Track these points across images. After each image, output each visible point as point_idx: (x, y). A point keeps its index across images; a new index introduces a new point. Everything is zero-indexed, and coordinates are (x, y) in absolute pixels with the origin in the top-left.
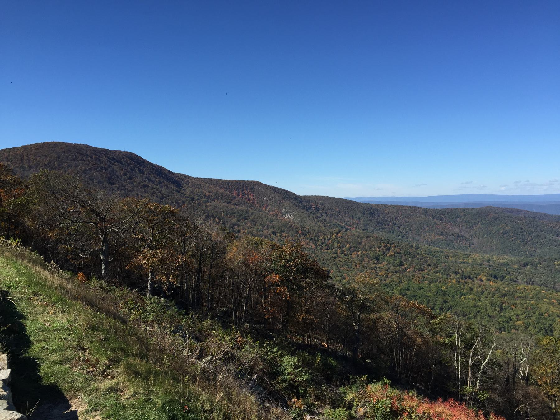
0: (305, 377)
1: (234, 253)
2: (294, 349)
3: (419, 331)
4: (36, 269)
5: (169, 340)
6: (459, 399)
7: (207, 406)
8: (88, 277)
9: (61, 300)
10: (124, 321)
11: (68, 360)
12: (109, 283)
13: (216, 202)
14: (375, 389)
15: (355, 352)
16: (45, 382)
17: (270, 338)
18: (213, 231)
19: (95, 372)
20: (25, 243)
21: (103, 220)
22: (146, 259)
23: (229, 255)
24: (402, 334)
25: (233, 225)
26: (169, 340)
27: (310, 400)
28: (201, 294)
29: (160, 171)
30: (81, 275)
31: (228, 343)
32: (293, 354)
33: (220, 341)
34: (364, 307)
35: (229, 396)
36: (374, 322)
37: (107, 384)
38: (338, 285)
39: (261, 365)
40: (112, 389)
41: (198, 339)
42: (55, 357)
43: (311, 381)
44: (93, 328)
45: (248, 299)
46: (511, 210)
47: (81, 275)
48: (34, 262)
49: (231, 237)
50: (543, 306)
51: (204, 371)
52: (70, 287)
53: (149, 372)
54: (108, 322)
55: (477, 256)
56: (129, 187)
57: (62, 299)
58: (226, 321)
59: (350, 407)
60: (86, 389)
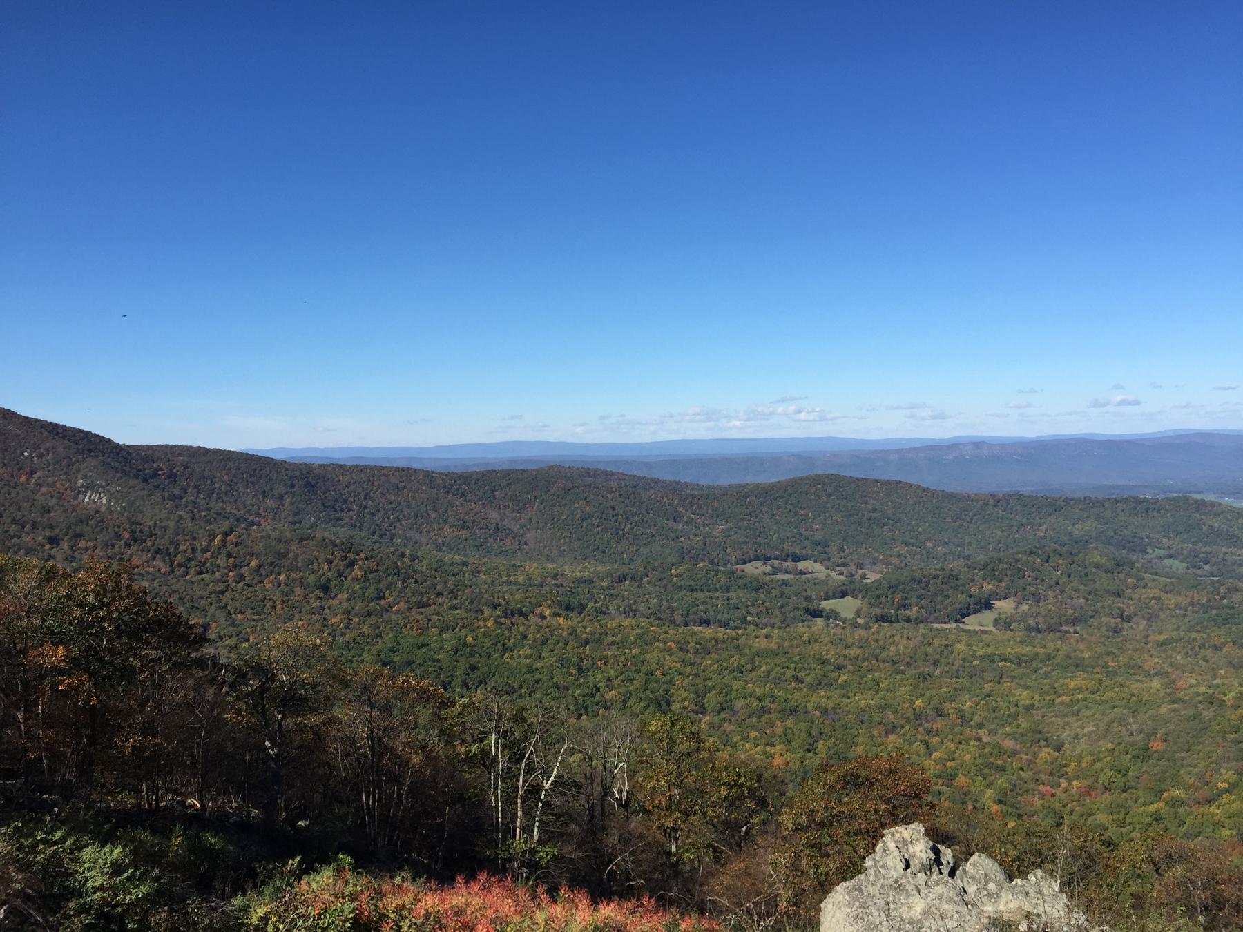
3: (417, 739)
6: (499, 869)
32: (106, 839)
34: (293, 701)
36: (316, 731)
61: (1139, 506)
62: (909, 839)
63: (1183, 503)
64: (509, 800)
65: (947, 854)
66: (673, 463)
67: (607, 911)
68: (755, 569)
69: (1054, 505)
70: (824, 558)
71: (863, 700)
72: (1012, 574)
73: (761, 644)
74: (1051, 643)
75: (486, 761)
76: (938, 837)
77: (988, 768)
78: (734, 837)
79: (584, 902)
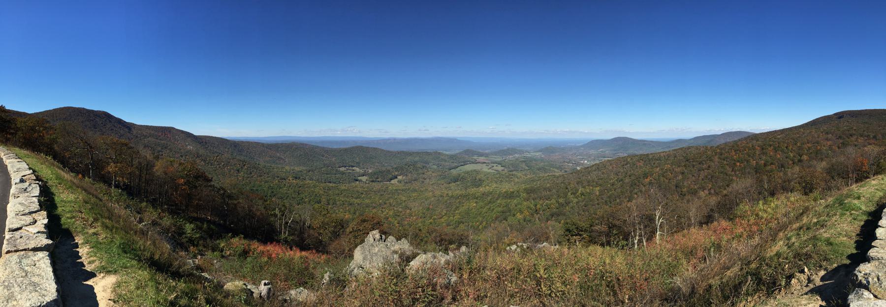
0: (198, 235)
1: (159, 168)
2: (192, 220)
3: (259, 208)
4: (59, 171)
5: (123, 212)
6: (278, 242)
7: (142, 247)
8: (84, 176)
9: (71, 187)
10: (101, 200)
11: (74, 217)
12: (94, 180)
13: (150, 139)
14: (235, 240)
15: (225, 221)
16: (63, 227)
17: (178, 214)
18: (148, 154)
19: (87, 225)
20: (54, 158)
21: (91, 147)
22: (111, 168)
23: (156, 168)
24: (250, 211)
25: (159, 152)
26: (123, 212)
27: (201, 248)
28: (140, 188)
29: (120, 121)
30: (80, 176)
31: (155, 216)
32: (191, 223)
33: (151, 214)
34: (230, 197)
35: (154, 243)
36: (235, 205)
37: (92, 231)
38: (216, 185)
39: (173, 229)
40: (94, 234)
41: (139, 213)
42: (68, 215)
43: (201, 237)
44: (86, 203)
45: (167, 192)
46: (302, 144)
47: (80, 176)
48: (59, 168)
49: (157, 158)
50: (317, 190)
51: (142, 230)
52: (75, 181)
53: (113, 227)
54: (93, 200)
55: (287, 168)
56: (104, 130)
57: (72, 187)
58: (154, 203)
59: (222, 251)
60: (82, 232)
61: (428, 154)
62: (376, 233)
63: (436, 153)
64: (281, 225)
65: (384, 237)
66: (323, 142)
67: (304, 253)
68: (342, 169)
69: (410, 154)
70: (358, 166)
71: (367, 201)
72: (401, 170)
73: (343, 188)
74: (408, 186)
75: (275, 215)
76: (383, 232)
77: (396, 215)
78: (336, 235)
79: (298, 251)
